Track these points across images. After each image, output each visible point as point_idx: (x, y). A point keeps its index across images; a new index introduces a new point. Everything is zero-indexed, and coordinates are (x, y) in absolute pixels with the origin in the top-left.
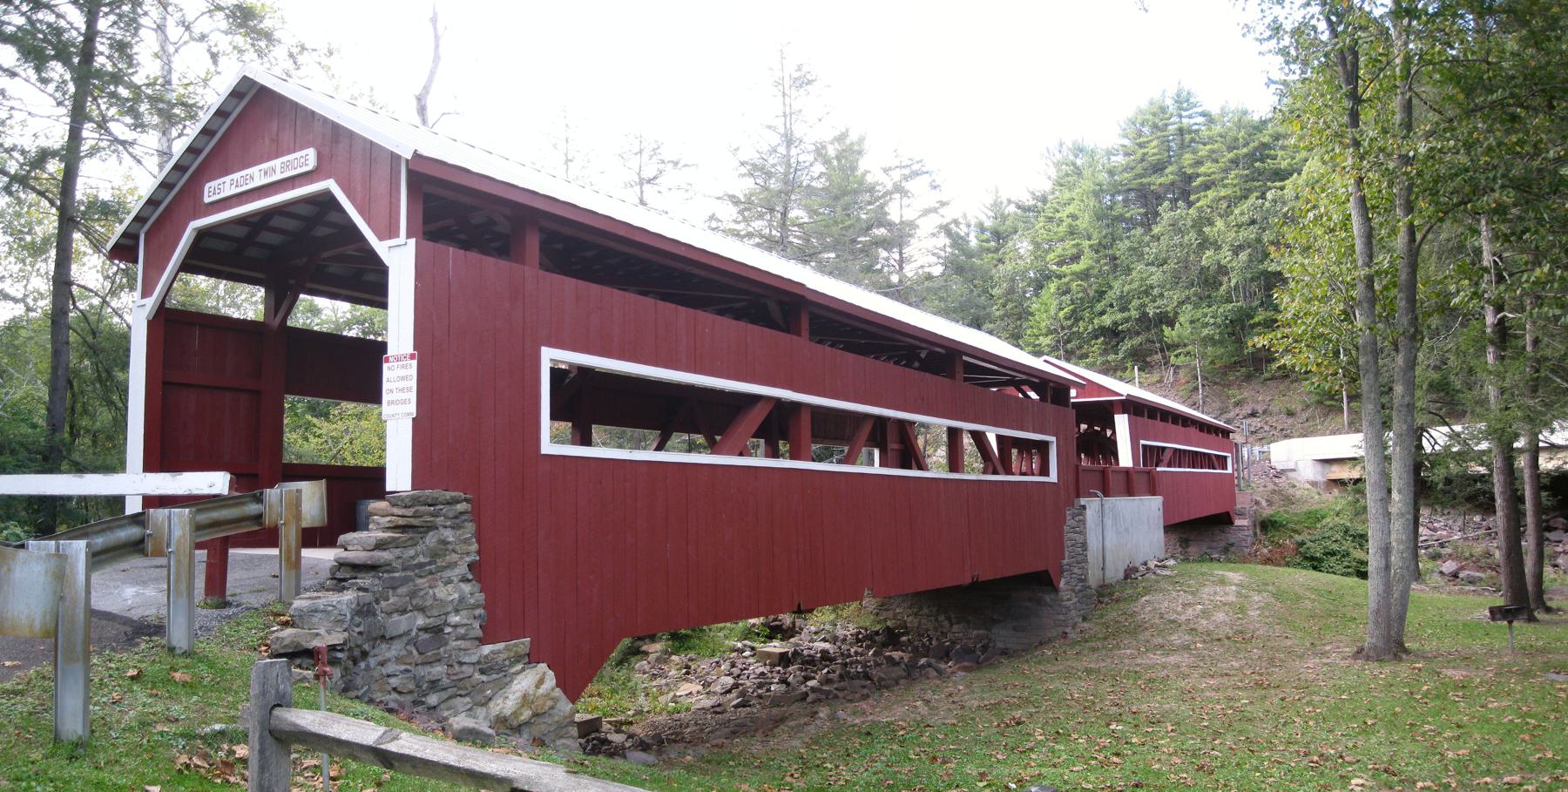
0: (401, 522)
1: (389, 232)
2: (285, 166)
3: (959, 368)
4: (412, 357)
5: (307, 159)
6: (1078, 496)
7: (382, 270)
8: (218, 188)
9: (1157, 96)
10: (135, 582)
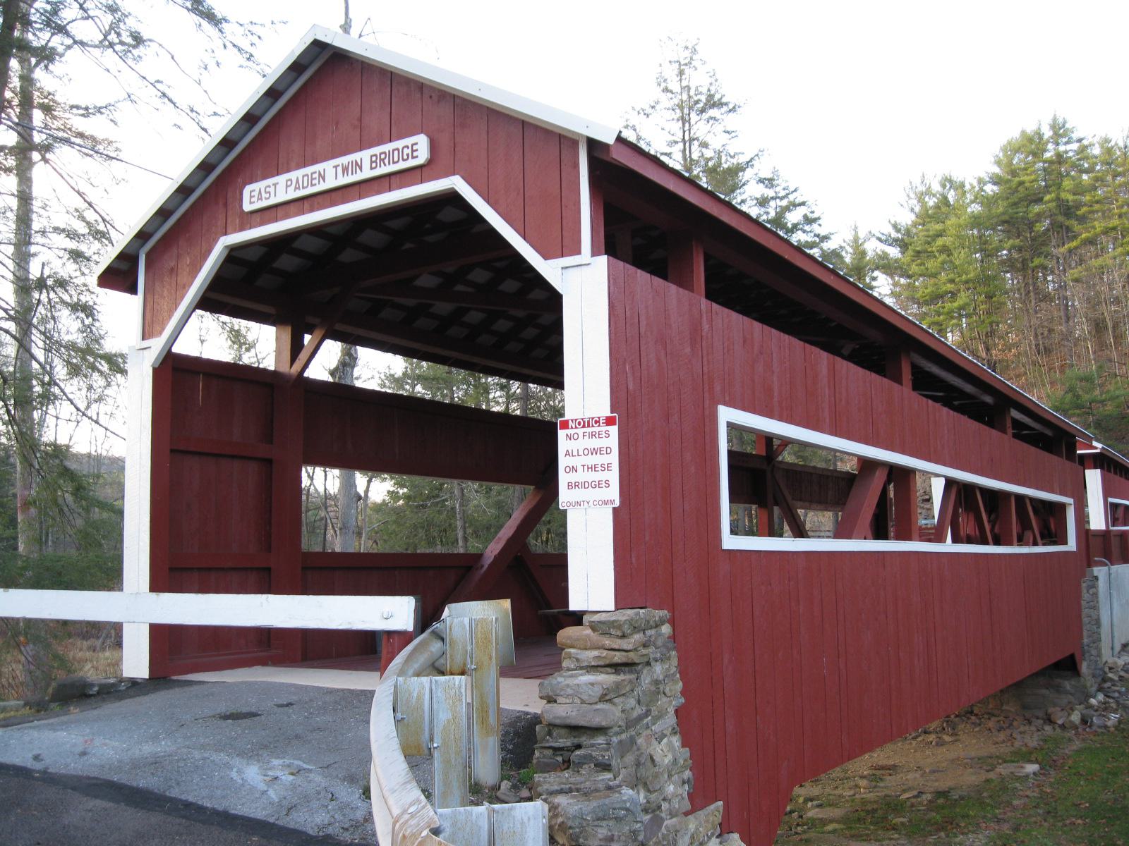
0: (618, 657)
1: (564, 245)
2: (376, 161)
3: (1009, 424)
4: (609, 421)
5: (419, 148)
6: (1089, 566)
7: (553, 300)
8: (255, 195)
9: (1030, 129)
10: (278, 758)
